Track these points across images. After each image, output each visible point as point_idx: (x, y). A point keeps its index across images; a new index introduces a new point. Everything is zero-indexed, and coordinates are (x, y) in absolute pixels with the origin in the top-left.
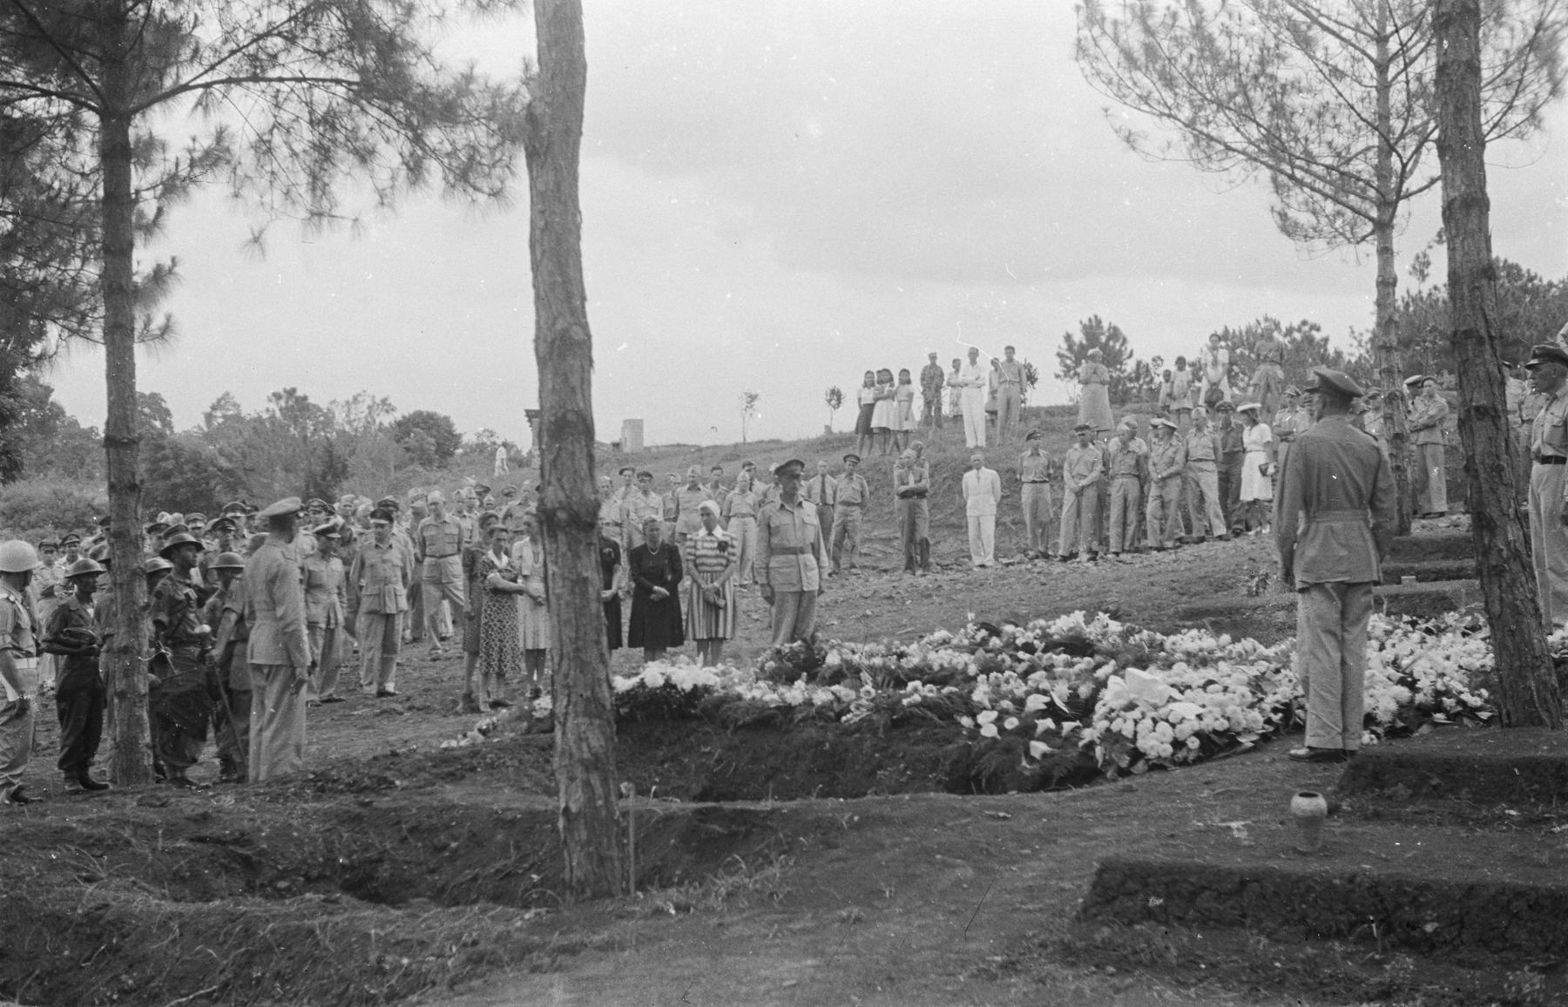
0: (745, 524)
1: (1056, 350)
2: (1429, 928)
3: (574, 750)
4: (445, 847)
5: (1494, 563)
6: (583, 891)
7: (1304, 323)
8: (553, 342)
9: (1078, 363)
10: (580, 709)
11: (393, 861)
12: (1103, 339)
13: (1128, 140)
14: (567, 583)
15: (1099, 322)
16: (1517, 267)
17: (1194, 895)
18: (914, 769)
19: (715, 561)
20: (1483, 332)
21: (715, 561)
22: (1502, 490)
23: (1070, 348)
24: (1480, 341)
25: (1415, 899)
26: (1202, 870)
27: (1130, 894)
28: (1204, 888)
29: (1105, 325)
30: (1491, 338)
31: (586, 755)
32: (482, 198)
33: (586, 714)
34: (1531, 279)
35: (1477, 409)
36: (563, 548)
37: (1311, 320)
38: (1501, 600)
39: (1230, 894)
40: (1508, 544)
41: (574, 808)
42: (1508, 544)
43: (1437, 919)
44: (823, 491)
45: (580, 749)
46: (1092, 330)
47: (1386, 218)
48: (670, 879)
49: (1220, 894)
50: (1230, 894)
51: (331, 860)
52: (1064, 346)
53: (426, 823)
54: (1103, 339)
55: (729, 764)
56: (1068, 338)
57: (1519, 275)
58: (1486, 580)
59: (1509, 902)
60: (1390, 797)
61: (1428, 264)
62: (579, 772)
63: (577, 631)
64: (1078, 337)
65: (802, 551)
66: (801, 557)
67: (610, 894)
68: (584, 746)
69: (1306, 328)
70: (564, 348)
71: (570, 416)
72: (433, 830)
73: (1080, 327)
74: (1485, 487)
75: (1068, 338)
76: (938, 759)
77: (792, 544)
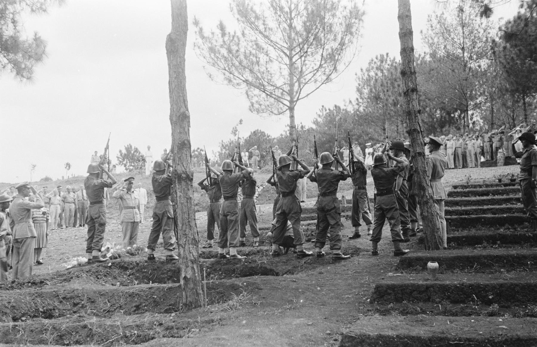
0: (57, 207)
1: (116, 155)
2: (490, 297)
3: (188, 256)
4: (78, 304)
5: (425, 200)
6: (192, 305)
7: (198, 149)
8: (179, 116)
9: (124, 160)
10: (190, 242)
11: (59, 309)
12: (132, 152)
13: (210, 77)
14: (185, 199)
15: (131, 147)
16: (264, 132)
17: (411, 293)
18: (225, 273)
19: (41, 219)
20: (419, 130)
21: (41, 219)
22: (427, 178)
23: (121, 155)
24: (419, 132)
25: (485, 289)
26: (413, 285)
27: (389, 294)
28: (414, 291)
29: (133, 148)
30: (421, 131)
31: (193, 258)
32: (25, 80)
33: (192, 244)
34: (268, 137)
35: (419, 153)
36: (184, 187)
37: (200, 148)
38: (428, 211)
39: (423, 292)
40: (429, 194)
41: (188, 277)
42: (429, 194)
43: (493, 294)
44: (83, 195)
45: (190, 256)
46: (128, 149)
47: (292, 106)
48: (178, 308)
49: (420, 292)
50: (423, 292)
51: (37, 310)
52: (119, 154)
53: (69, 296)
54: (132, 152)
55: (154, 276)
56: (120, 151)
57: (265, 136)
58: (87, 268)
59: (514, 288)
60: (415, 270)
61: (236, 131)
62: (190, 264)
63: (189, 215)
64: (124, 151)
65: (134, 208)
66: (134, 210)
67: (200, 306)
68: (191, 255)
69: (199, 150)
70: (180, 119)
71: (186, 142)
72: (71, 298)
73: (124, 148)
74: (422, 177)
75: (120, 151)
76: (234, 269)
77: (131, 205)
